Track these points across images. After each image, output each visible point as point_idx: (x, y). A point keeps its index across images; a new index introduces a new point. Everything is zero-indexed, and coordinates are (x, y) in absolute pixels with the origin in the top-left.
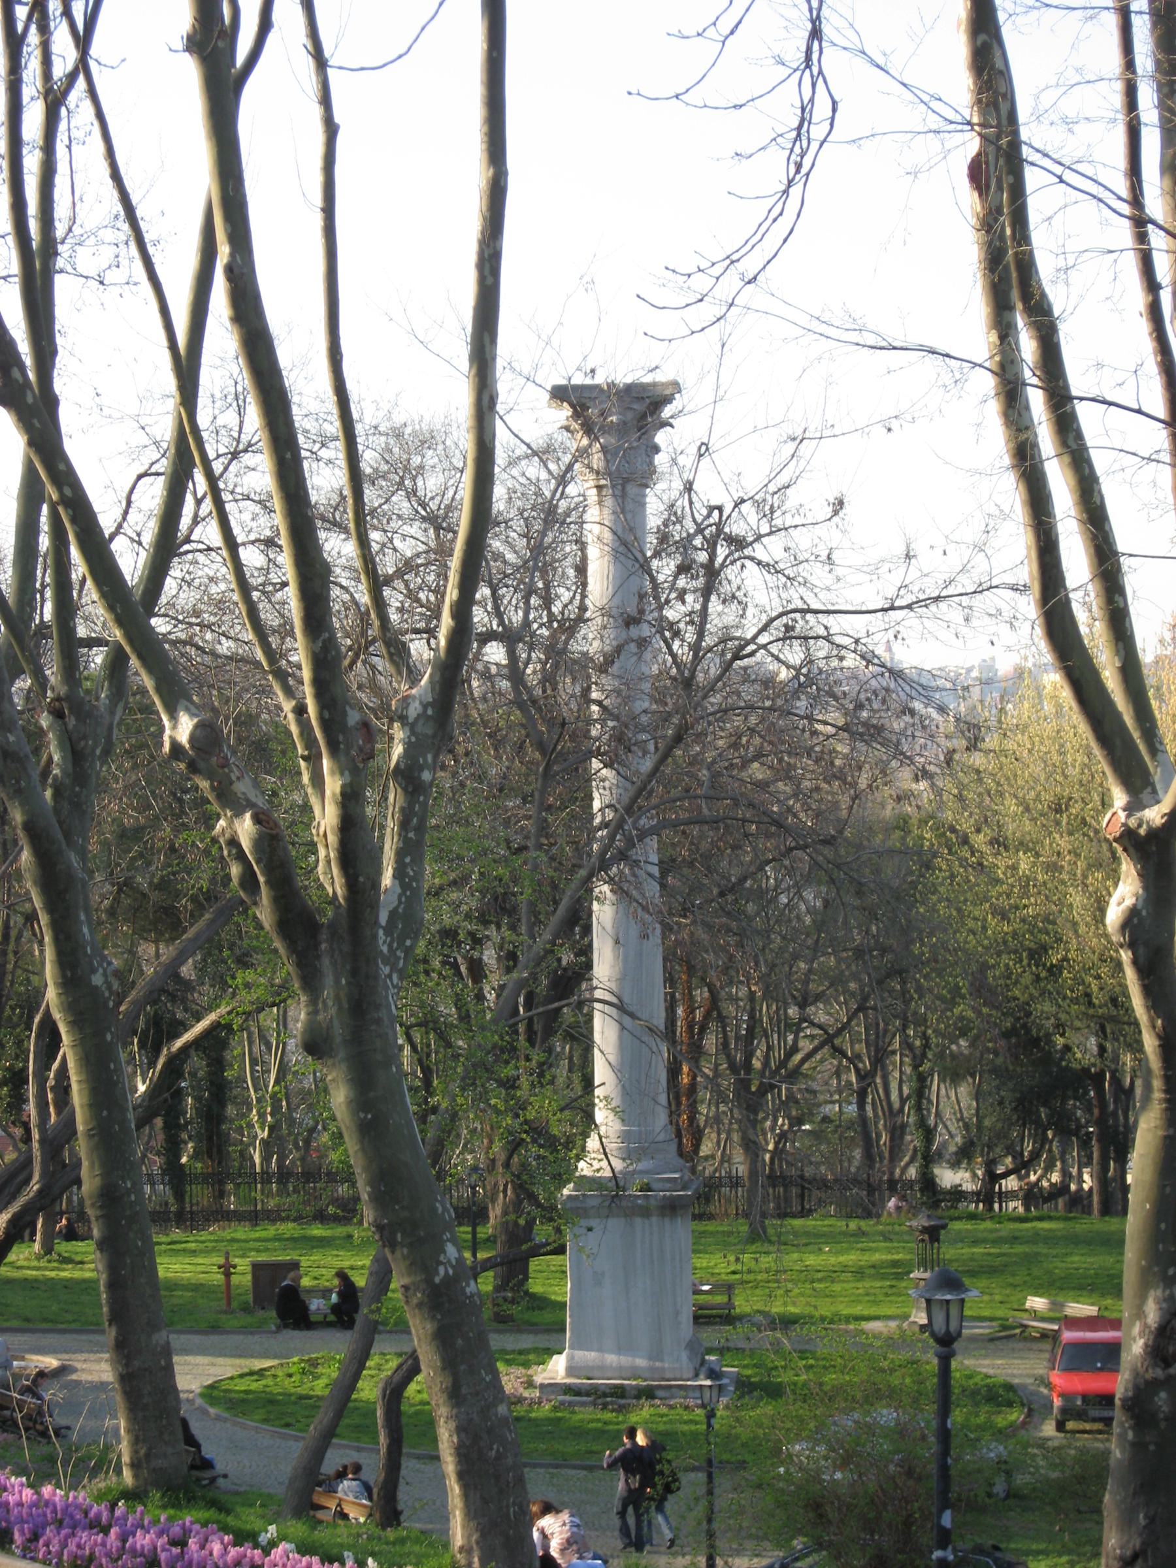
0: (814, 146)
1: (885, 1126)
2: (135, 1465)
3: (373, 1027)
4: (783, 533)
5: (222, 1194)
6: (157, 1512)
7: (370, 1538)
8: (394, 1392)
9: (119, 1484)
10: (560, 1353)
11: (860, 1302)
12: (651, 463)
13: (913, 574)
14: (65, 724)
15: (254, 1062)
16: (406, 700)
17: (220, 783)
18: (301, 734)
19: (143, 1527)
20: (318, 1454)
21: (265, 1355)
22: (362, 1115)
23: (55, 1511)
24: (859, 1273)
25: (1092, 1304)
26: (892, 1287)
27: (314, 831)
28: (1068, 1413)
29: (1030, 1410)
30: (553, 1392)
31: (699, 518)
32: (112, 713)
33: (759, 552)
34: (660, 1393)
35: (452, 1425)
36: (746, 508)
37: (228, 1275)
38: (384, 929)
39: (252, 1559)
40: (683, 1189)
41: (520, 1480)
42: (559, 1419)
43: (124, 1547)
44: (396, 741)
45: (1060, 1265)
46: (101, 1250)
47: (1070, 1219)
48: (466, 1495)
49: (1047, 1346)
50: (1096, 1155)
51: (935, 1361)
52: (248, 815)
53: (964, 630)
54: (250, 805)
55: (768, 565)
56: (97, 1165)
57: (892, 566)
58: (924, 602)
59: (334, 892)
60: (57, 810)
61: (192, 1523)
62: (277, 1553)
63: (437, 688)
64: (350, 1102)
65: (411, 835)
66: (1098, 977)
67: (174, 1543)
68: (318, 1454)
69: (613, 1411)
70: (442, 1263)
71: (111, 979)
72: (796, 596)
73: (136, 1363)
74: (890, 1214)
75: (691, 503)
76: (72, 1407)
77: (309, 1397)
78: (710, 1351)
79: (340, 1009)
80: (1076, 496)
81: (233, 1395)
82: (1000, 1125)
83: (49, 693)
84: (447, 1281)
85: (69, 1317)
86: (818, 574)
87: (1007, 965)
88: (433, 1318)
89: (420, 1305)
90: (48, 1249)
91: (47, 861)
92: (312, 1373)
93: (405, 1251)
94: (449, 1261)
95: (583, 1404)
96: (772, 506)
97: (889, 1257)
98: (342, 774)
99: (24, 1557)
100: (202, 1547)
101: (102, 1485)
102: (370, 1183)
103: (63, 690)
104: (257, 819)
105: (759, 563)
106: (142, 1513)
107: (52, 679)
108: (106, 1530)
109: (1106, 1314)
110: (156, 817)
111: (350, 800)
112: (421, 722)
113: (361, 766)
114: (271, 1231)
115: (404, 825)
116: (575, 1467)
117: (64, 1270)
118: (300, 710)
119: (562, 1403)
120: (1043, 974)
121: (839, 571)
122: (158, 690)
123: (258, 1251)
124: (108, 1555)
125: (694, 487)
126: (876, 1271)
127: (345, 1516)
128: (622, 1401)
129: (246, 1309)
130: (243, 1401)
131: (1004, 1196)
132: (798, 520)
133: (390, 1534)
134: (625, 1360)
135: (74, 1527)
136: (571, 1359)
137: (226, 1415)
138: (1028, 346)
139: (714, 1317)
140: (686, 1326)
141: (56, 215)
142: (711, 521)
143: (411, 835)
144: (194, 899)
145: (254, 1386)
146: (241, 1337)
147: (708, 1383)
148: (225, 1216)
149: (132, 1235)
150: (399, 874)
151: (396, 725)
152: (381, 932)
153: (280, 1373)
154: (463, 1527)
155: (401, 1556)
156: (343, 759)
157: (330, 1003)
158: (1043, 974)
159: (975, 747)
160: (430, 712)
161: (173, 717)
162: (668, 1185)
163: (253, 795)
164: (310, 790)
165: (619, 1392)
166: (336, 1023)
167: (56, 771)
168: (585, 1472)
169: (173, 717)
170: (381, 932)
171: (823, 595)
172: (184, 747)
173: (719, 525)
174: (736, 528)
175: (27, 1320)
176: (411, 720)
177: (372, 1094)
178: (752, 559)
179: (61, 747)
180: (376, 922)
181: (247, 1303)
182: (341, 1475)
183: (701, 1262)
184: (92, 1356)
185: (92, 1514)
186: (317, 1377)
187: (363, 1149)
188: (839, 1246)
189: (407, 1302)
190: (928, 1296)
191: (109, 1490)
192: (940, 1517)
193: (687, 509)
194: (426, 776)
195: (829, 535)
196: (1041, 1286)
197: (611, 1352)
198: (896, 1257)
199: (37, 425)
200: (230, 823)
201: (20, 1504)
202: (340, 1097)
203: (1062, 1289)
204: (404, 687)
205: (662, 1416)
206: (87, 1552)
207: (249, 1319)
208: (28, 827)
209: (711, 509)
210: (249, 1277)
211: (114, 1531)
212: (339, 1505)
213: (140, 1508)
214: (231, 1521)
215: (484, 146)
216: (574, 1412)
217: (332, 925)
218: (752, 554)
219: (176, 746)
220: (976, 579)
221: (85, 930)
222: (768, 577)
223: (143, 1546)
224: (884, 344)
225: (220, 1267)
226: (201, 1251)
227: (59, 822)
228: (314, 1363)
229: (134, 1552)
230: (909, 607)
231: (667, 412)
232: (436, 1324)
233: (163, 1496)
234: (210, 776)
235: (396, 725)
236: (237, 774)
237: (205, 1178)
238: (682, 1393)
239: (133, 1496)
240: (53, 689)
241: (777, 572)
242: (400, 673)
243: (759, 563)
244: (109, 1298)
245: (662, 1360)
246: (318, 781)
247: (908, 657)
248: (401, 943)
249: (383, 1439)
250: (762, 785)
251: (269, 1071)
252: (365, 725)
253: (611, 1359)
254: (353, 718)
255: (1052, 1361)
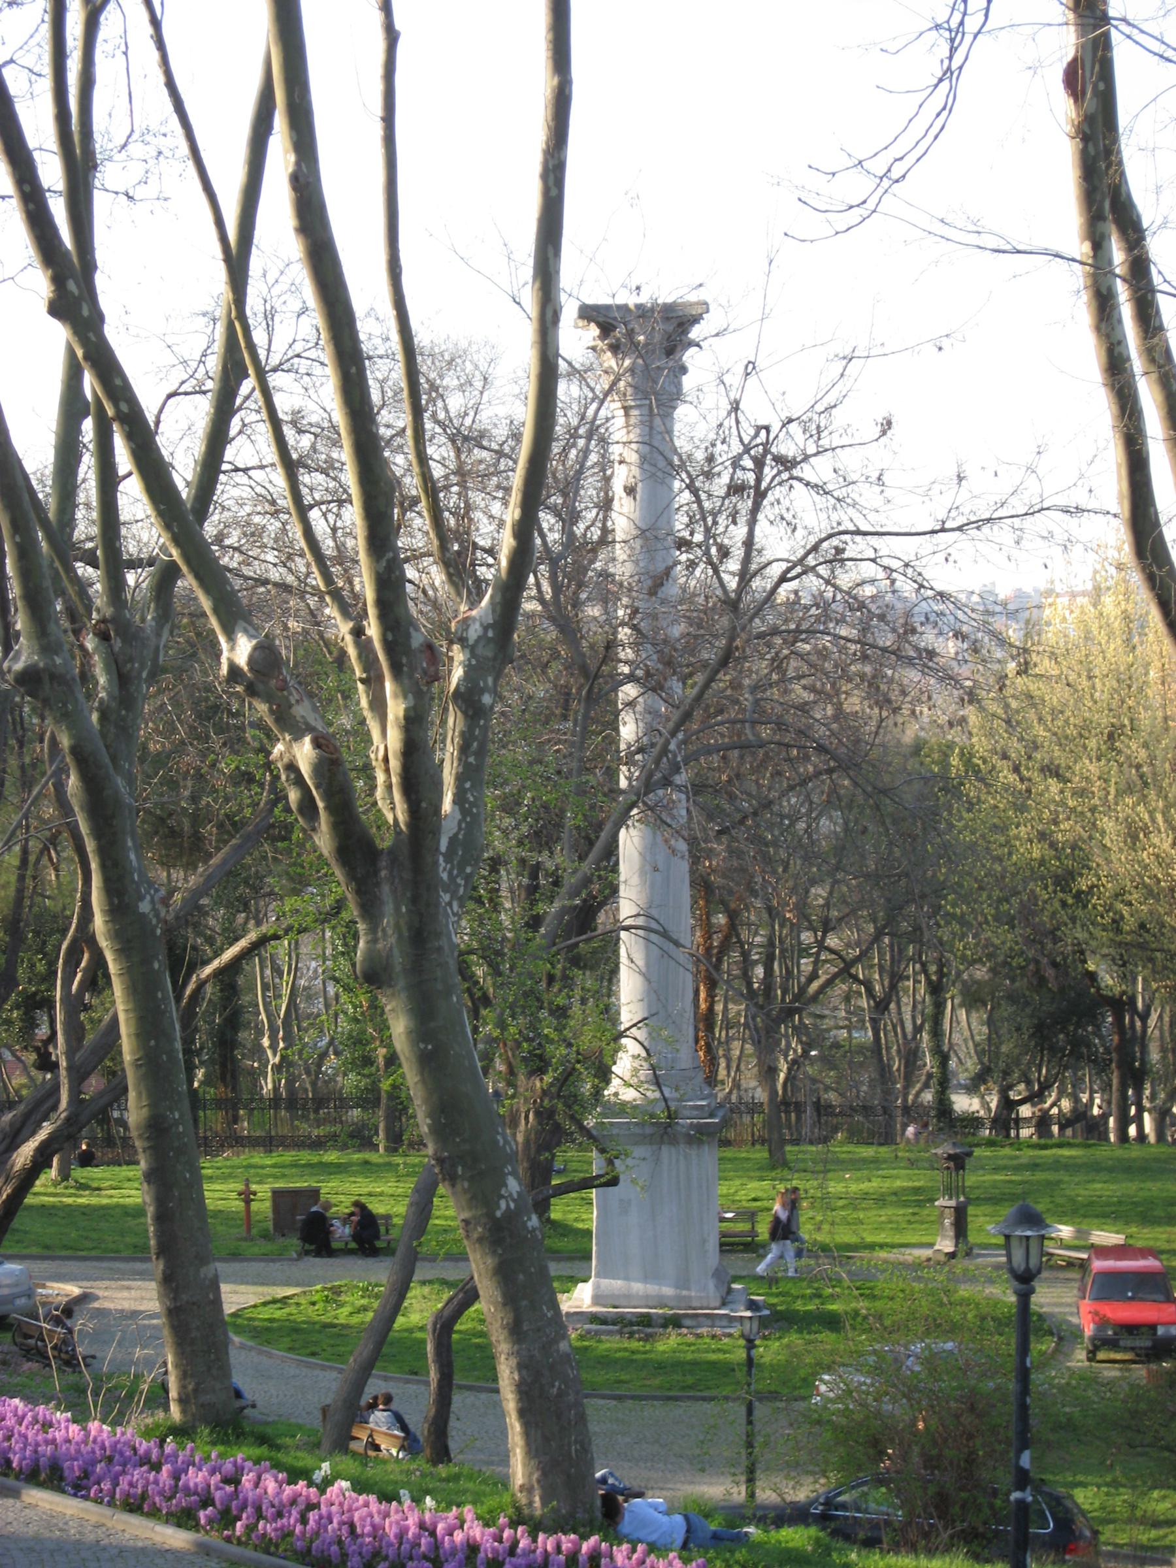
0: (968, 38)
1: (899, 1051)
2: (183, 1401)
3: (434, 956)
4: (829, 453)
5: (236, 1119)
6: (207, 1448)
7: (423, 1475)
8: (445, 1325)
9: (166, 1419)
10: (585, 1281)
11: (883, 1229)
12: (679, 386)
13: (964, 494)
14: (111, 646)
15: (265, 987)
16: (466, 622)
17: (279, 706)
18: (360, 656)
19: (194, 1465)
20: (358, 1385)
21: (287, 1283)
22: (422, 1046)
23: (103, 1448)
24: (881, 1200)
25: (1118, 1232)
26: (914, 1214)
27: (372, 756)
28: (1099, 1343)
29: (1061, 1339)
30: (579, 1321)
31: (746, 440)
32: (159, 635)
33: (805, 471)
34: (687, 1322)
35: (513, 1362)
36: (794, 428)
37: (248, 1202)
38: (444, 855)
39: (308, 1497)
40: (711, 1116)
41: (582, 1418)
42: (586, 1348)
43: (176, 1486)
44: (456, 663)
45: (1082, 1192)
46: (149, 1182)
47: (1089, 1146)
48: (527, 1434)
49: (1075, 1275)
50: (1115, 1082)
51: (1013, 1299)
52: (307, 740)
53: (1015, 553)
54: (310, 729)
55: (817, 486)
56: (144, 1096)
57: (944, 488)
58: (980, 523)
59: (396, 819)
60: (103, 734)
61: (244, 1460)
62: (333, 1491)
63: (498, 609)
64: (409, 1033)
65: (471, 759)
66: (1130, 904)
67: (227, 1481)
68: (358, 1385)
69: (640, 1340)
70: (503, 1197)
71: (159, 906)
72: (845, 518)
73: (184, 1297)
74: (908, 1141)
75: (738, 422)
76: (100, 1337)
77: (334, 1326)
78: (736, 1279)
79: (400, 937)
80: (1163, 412)
81: (256, 1323)
82: (1017, 1051)
83: (94, 615)
84: (509, 1215)
85: (88, 1244)
86: (867, 495)
87: (1032, 891)
88: (494, 1252)
89: (480, 1240)
90: (65, 1175)
91: (93, 785)
92: (335, 1301)
93: (466, 1184)
94: (511, 1195)
95: (610, 1333)
96: (818, 427)
97: (910, 1184)
98: (405, 697)
99: (75, 1495)
100: (257, 1485)
101: (149, 1421)
102: (430, 1115)
103: (109, 612)
104: (317, 744)
105: (807, 484)
106: (192, 1450)
107: (98, 602)
108: (156, 1467)
109: (1131, 1242)
110: (182, 742)
111: (414, 724)
112: (481, 645)
113: (425, 689)
114: (288, 1156)
115: (464, 749)
116: (603, 1397)
117: (81, 1196)
118: (358, 632)
119: (589, 1332)
120: (1070, 901)
121: (889, 493)
122: (216, 610)
123: (275, 1177)
124: (161, 1493)
125: (741, 406)
126: (898, 1198)
127: (377, 1448)
128: (649, 1330)
129: (265, 1236)
130: (268, 1329)
131: (1019, 1123)
132: (845, 441)
133: (443, 1470)
134: (652, 1289)
135: (124, 1465)
136: (597, 1287)
137: (250, 1343)
138: (1118, 256)
139: (738, 1244)
140: (713, 1256)
141: (32, 142)
142: (758, 441)
143: (471, 759)
144: (220, 826)
145: (278, 1314)
146: (263, 1264)
147: (748, 1314)
148: (238, 1142)
149: (179, 1167)
150: (458, 800)
151: (456, 647)
152: (441, 859)
153: (303, 1301)
154: (524, 1465)
155: (457, 1493)
156: (406, 681)
157: (390, 931)
158: (1070, 901)
159: (1026, 672)
160: (490, 634)
161: (231, 638)
162: (695, 1113)
163: (313, 719)
164: (367, 714)
165: (645, 1321)
166: (396, 952)
167: (103, 695)
168: (614, 1403)
169: (231, 638)
170: (441, 859)
171: (872, 517)
172: (241, 670)
173: (766, 445)
174: (786, 448)
175: (47, 1247)
176: (471, 642)
177: (432, 1025)
178: (800, 480)
179: (107, 669)
180: (437, 849)
181: (267, 1230)
182: (373, 1406)
183: (723, 1189)
184: (113, 1284)
185: (141, 1451)
186: (340, 1305)
187: (423, 1081)
188: (859, 1174)
189: (468, 1237)
190: (1007, 1232)
191: (157, 1425)
192: (1018, 1457)
193: (734, 430)
194: (487, 699)
195: (878, 456)
196: (1064, 1214)
197: (637, 1280)
198: (917, 1184)
199: (93, 339)
200: (289, 748)
201: (68, 1441)
202: (399, 1027)
203: (1085, 1216)
204: (463, 608)
205: (690, 1345)
206: (140, 1491)
207: (268, 1247)
208: (75, 751)
209: (758, 429)
210: (268, 1204)
211: (166, 1468)
212: (371, 1436)
213: (190, 1445)
214: (280, 1456)
215: (550, 54)
216: (599, 1341)
217: (391, 851)
218: (800, 475)
219: (234, 669)
220: (1027, 501)
221: (132, 856)
222: (817, 498)
223: (196, 1485)
224: (1008, 247)
225: (240, 1194)
226: (218, 1178)
227: (107, 747)
228: (337, 1291)
229: (187, 1491)
230: (960, 529)
231: (695, 333)
232: (497, 1260)
233: (211, 1432)
234: (268, 698)
235: (456, 647)
236: (297, 697)
237: (219, 1103)
238: (709, 1322)
239: (181, 1432)
240: (98, 610)
241: (826, 493)
242: (459, 594)
243: (807, 484)
244: (156, 1231)
245: (688, 1289)
246: (378, 704)
247: (941, 578)
248: (461, 869)
249: (433, 1375)
250: (804, 708)
251: (280, 996)
252: (430, 647)
253: (638, 1287)
254: (417, 641)
255: (1082, 1290)
